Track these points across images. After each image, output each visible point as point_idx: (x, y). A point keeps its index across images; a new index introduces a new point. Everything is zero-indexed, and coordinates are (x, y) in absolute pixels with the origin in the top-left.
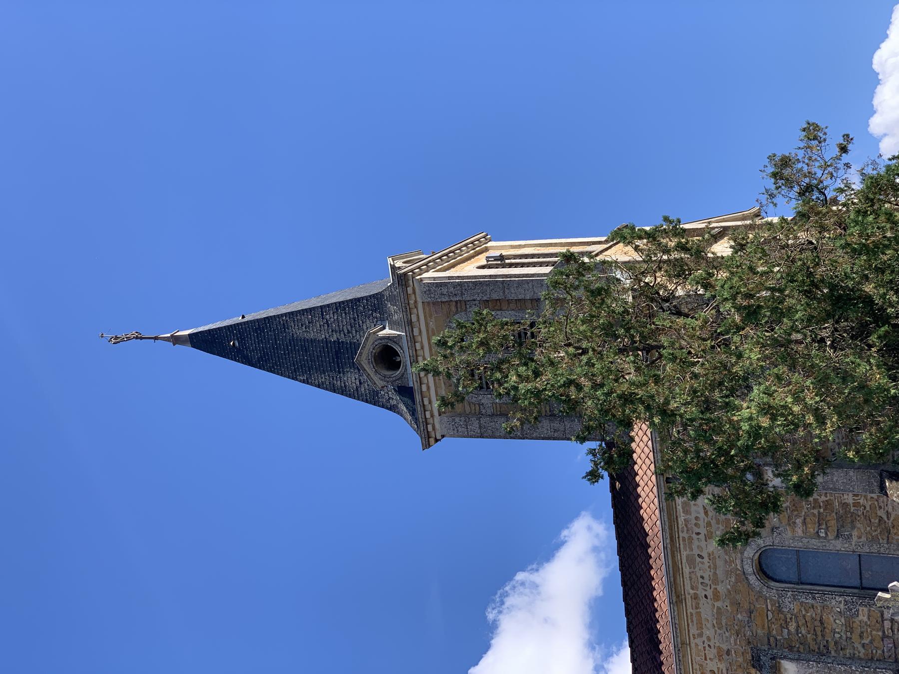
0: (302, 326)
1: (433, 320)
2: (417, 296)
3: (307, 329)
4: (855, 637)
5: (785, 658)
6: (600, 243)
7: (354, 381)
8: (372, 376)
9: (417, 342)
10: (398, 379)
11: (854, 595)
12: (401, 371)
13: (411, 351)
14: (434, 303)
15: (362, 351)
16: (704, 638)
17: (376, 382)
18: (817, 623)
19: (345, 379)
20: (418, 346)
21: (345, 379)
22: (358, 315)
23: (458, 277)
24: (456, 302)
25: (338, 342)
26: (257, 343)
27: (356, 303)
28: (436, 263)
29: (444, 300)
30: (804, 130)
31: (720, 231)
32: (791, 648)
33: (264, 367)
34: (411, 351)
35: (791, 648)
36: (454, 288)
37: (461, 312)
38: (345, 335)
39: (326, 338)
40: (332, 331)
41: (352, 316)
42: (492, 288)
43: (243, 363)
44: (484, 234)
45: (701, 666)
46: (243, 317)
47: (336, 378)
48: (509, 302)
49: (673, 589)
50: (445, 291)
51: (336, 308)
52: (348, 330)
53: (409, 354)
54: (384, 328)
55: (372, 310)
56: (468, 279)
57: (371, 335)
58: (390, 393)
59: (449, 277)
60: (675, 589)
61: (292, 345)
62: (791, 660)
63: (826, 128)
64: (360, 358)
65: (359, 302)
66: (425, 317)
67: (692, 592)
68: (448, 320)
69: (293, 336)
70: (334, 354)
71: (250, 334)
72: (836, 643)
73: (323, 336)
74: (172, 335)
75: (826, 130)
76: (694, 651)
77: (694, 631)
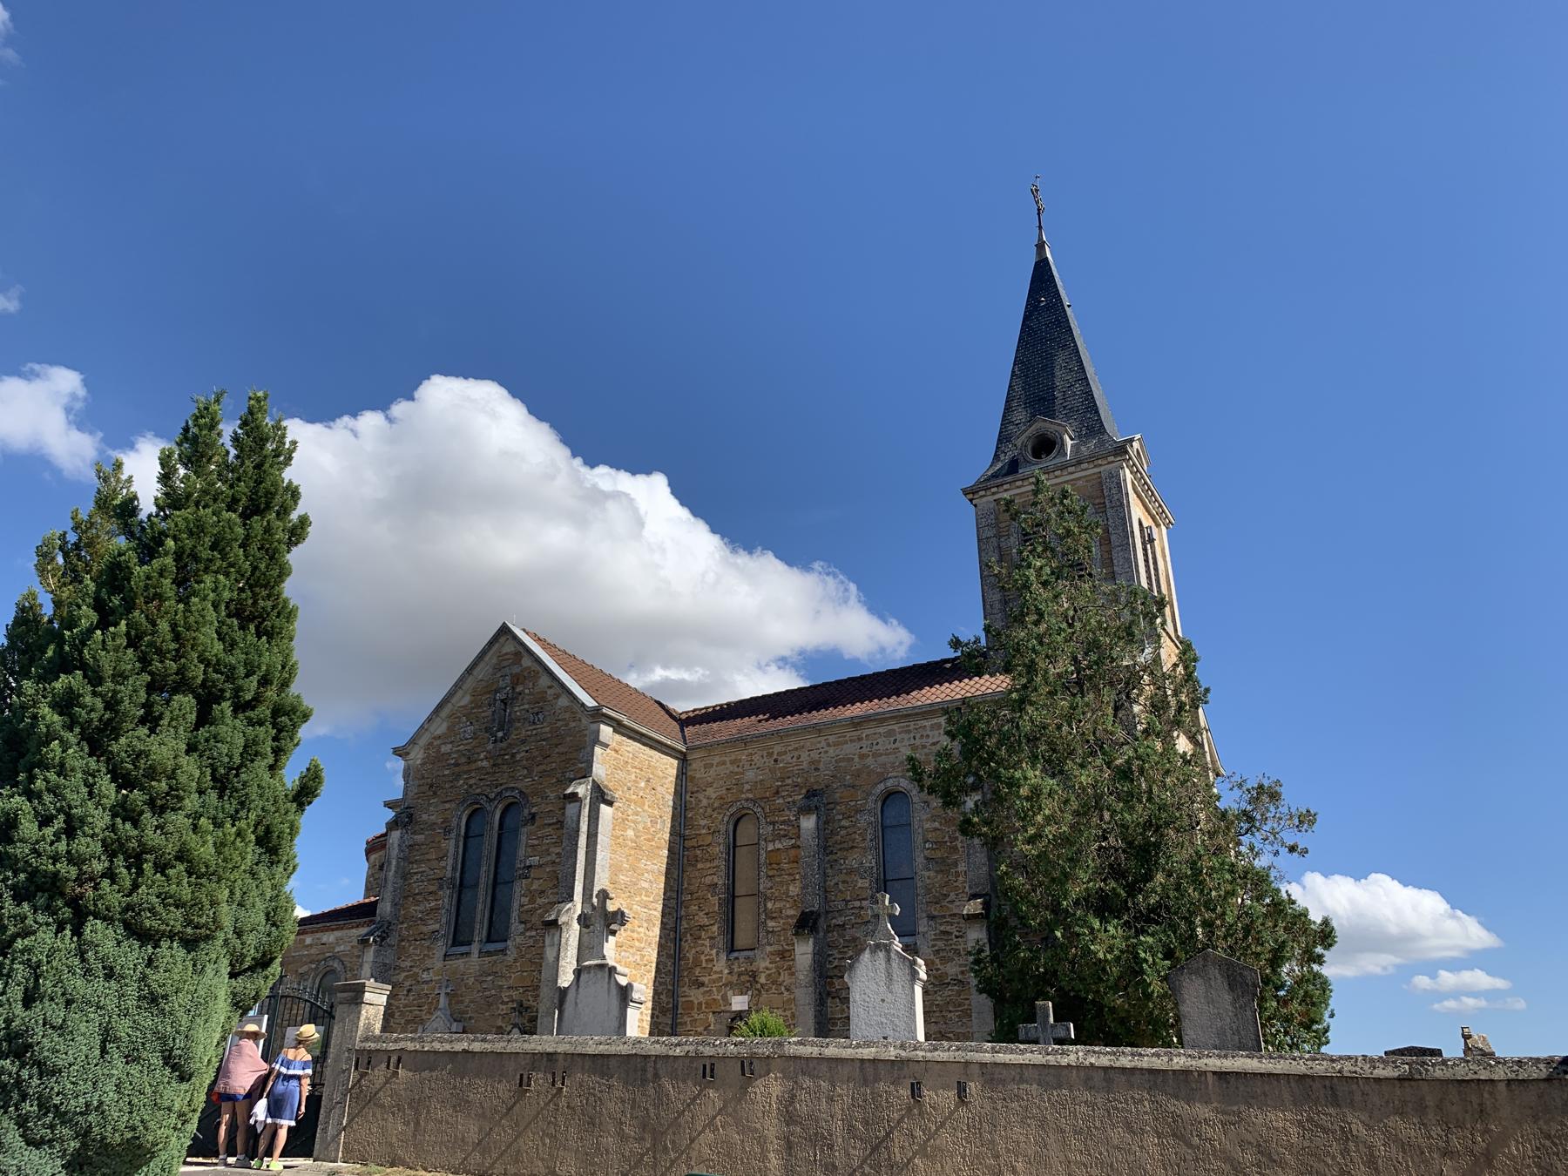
4: (843, 877)
5: (818, 818)
6: (1176, 630)
11: (878, 874)
14: (1100, 483)
18: (850, 844)
24: (1104, 503)
32: (827, 822)
35: (827, 822)
46: (1069, 306)
48: (1110, 552)
50: (1114, 491)
54: (1072, 439)
62: (817, 823)
77: (832, 739)
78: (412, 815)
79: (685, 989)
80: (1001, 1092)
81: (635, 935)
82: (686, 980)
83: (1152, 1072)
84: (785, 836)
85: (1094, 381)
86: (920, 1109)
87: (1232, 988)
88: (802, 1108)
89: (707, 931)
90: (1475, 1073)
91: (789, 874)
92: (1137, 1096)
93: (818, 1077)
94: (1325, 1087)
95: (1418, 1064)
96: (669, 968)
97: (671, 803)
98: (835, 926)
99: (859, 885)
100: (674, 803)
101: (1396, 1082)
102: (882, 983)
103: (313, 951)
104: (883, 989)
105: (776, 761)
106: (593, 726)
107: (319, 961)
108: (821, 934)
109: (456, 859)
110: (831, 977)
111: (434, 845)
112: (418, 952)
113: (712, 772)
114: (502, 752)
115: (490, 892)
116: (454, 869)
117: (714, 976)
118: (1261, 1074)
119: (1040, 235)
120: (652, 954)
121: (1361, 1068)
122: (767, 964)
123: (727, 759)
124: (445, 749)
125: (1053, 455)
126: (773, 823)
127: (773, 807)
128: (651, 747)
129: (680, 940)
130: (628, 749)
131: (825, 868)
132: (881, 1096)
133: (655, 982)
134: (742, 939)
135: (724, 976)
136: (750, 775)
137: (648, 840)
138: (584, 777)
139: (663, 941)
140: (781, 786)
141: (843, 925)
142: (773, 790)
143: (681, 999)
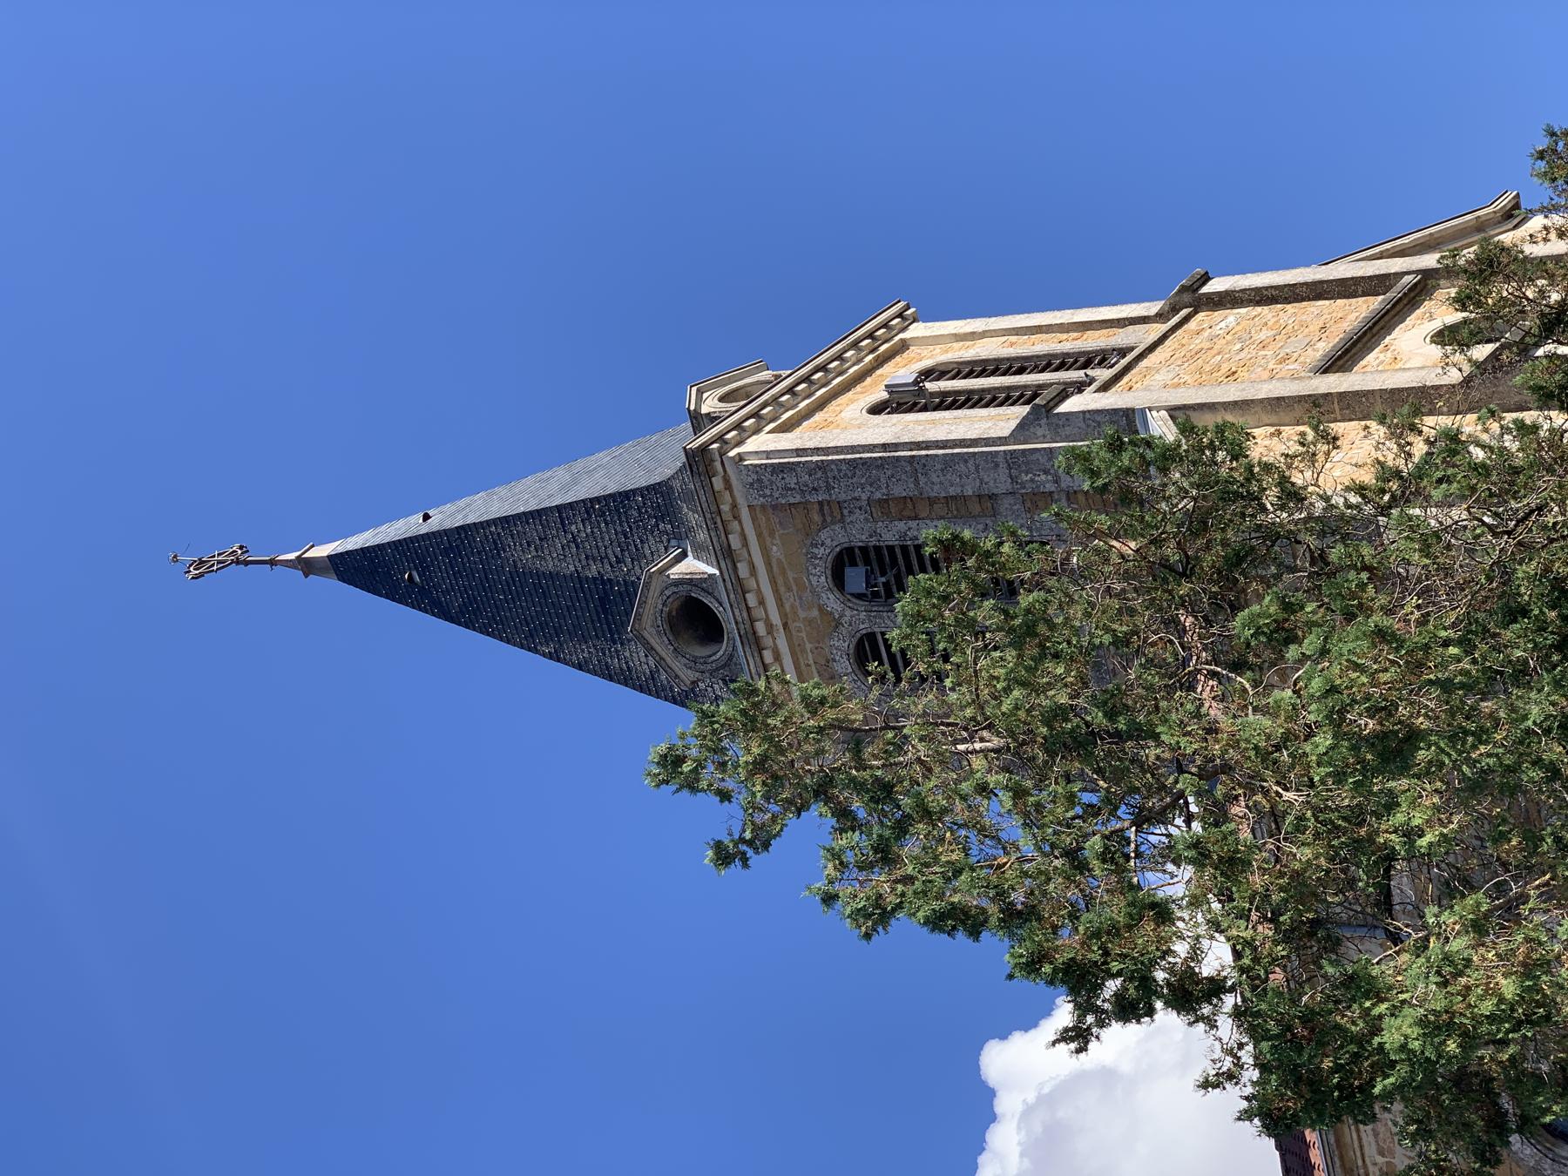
0: (529, 545)
1: (777, 541)
2: (736, 493)
3: (540, 553)
7: (643, 659)
8: (668, 660)
9: (749, 592)
10: (723, 667)
12: (726, 650)
13: (737, 612)
14: (774, 507)
15: (641, 610)
17: (680, 673)
19: (627, 654)
20: (752, 600)
21: (627, 654)
22: (630, 527)
23: (817, 451)
24: (820, 503)
25: (600, 580)
26: (452, 578)
27: (622, 502)
28: (781, 405)
29: (792, 500)
30: (1541, 155)
31: (1416, 284)
33: (474, 626)
34: (737, 612)
36: (810, 475)
37: (833, 523)
38: (612, 566)
39: (577, 571)
40: (587, 558)
41: (619, 529)
42: (889, 473)
46: (426, 517)
47: (610, 651)
48: (932, 501)
49: (1336, 1159)
50: (791, 481)
51: (587, 512)
52: (617, 557)
53: (735, 618)
54: (684, 555)
55: (656, 518)
56: (838, 453)
58: (716, 686)
59: (797, 450)
60: (1341, 1158)
61: (518, 584)
64: (639, 625)
65: (629, 500)
66: (759, 536)
67: (1380, 1159)
68: (808, 542)
69: (516, 566)
70: (597, 603)
71: (437, 559)
73: (572, 568)
85: (565, 488)
119: (287, 563)
125: (714, 606)
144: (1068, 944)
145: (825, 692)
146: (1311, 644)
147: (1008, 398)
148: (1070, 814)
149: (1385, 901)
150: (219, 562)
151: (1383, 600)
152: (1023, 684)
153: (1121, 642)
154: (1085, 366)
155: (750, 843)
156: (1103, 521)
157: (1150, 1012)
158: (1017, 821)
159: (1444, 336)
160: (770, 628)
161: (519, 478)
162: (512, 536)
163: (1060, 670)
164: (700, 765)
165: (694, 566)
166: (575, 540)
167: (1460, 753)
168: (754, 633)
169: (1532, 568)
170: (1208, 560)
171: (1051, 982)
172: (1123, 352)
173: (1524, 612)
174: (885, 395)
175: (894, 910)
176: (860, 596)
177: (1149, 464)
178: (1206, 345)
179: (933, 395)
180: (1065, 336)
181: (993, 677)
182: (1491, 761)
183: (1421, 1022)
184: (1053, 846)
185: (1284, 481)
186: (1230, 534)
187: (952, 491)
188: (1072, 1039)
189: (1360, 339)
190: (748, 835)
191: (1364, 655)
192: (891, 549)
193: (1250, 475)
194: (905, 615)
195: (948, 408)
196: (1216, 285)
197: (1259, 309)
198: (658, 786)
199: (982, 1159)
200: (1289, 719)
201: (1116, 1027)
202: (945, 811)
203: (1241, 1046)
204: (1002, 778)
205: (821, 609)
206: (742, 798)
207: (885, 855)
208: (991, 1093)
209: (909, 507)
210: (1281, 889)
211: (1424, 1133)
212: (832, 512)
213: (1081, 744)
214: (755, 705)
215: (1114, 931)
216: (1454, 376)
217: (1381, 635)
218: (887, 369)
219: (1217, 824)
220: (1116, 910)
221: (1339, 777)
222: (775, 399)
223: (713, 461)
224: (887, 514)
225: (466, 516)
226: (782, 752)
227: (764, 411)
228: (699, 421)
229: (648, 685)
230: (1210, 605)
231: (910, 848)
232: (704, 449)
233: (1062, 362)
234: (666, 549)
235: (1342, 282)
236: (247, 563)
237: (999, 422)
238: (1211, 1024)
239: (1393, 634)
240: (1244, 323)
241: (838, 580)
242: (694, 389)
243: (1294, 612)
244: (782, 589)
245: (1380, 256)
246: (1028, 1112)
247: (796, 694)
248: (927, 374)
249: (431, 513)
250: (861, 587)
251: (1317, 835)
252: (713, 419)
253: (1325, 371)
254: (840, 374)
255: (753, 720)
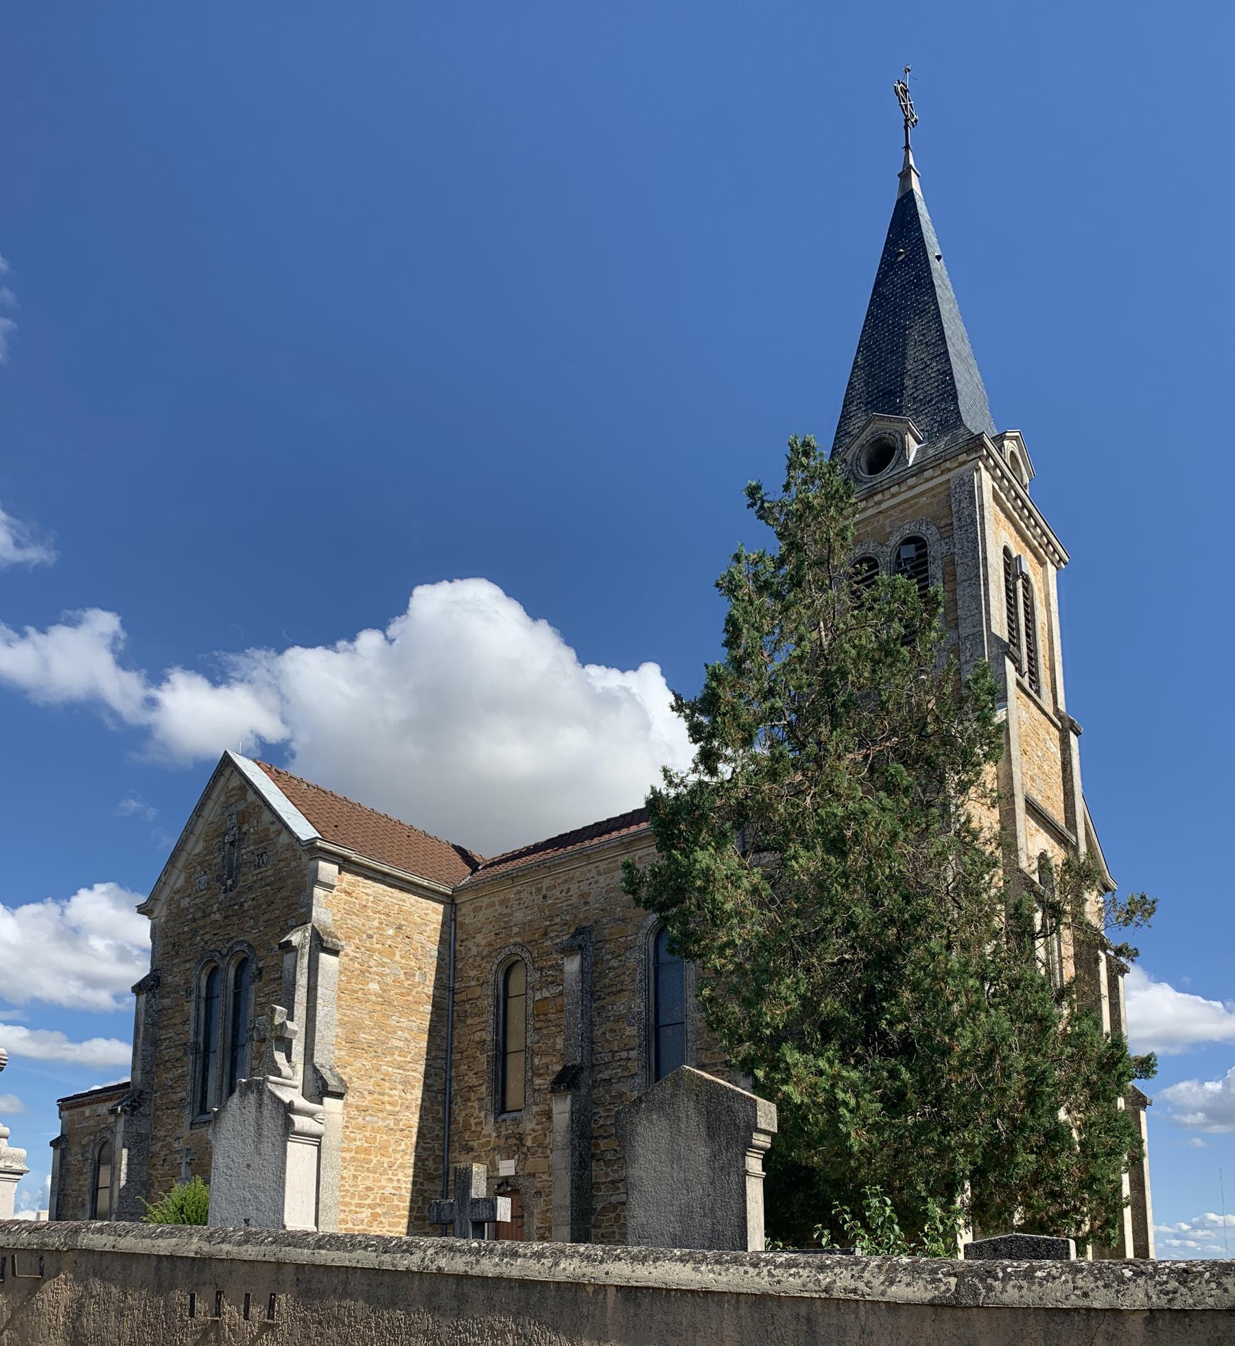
1: (929, 501)
4: (610, 1025)
5: (583, 959)
6: (1055, 702)
11: (648, 1020)
14: (949, 495)
16: (597, 878)
18: (619, 987)
20: (894, 489)
23: (983, 517)
24: (952, 524)
28: (1009, 492)
32: (595, 964)
35: (595, 964)
37: (940, 533)
43: (878, 275)
44: (1067, 559)
45: (573, 879)
46: (939, 258)
48: (954, 591)
51: (944, 372)
54: (919, 442)
57: (906, 425)
62: (582, 964)
63: (1149, 926)
66: (932, 488)
67: (636, 858)
72: (603, 1007)
73: (910, 367)
74: (911, 166)
75: (1145, 926)
76: (584, 868)
77: (602, 866)
78: (159, 977)
79: (455, 1154)
80: (317, 1311)
81: (386, 1098)
82: (457, 1144)
83: (525, 1284)
84: (552, 983)
85: (959, 354)
86: (217, 1334)
87: (712, 1134)
88: (88, 1324)
89: (476, 1092)
90: (1086, 1295)
91: (557, 1026)
92: (497, 1326)
93: (111, 1281)
94: (797, 1317)
95: (977, 1275)
96: (437, 1132)
97: (436, 953)
98: (601, 1080)
99: (627, 1033)
100: (439, 952)
101: (930, 1310)
102: (249, 1141)
103: (92, 1122)
104: (250, 1149)
105: (545, 897)
106: (312, 863)
107: (96, 1133)
108: (584, 1091)
109: (197, 1023)
110: (596, 1138)
111: (178, 1008)
112: (170, 1121)
113: (481, 916)
114: (232, 902)
115: (228, 1055)
116: (197, 1034)
117: (483, 1140)
118: (692, 1291)
120: (413, 1119)
121: (867, 1284)
122: (533, 1125)
123: (496, 900)
124: (185, 903)
125: (890, 466)
126: (541, 969)
127: (541, 951)
128: (402, 889)
129: (451, 1102)
130: (367, 891)
131: (592, 1016)
132: (174, 1311)
133: (417, 1147)
134: (511, 1103)
135: (493, 1140)
136: (519, 916)
137: (402, 994)
138: (305, 923)
139: (427, 1104)
140: (550, 926)
141: (610, 1079)
142: (541, 931)
143: (452, 1165)
144: (726, 695)
145: (850, 540)
146: (888, 802)
147: (1013, 629)
148: (791, 688)
149: (759, 850)
150: (906, 106)
151: (911, 836)
152: (859, 654)
153: (883, 705)
154: (1031, 672)
155: (762, 507)
156: (948, 689)
157: (695, 741)
158: (785, 660)
159: (1043, 856)
160: (879, 503)
161: (963, 321)
162: (928, 322)
163: (866, 674)
164: (805, 467)
165: (913, 448)
166: (926, 366)
167: (836, 878)
168: (876, 494)
169: (931, 905)
170: (928, 748)
171: (706, 686)
172: (1038, 692)
173: (908, 903)
174: (1014, 555)
175: (735, 596)
176: (898, 556)
177: (981, 710)
178: (1041, 738)
179: (1015, 584)
180: (1047, 658)
181: (860, 637)
182: (834, 892)
183: (708, 868)
184: (775, 680)
185: (971, 782)
186: (942, 758)
187: (960, 602)
188: (677, 703)
189: (1043, 817)
190: (766, 505)
191: (884, 828)
192: (926, 570)
193: (975, 765)
194: (895, 580)
195: (1007, 595)
196: (1073, 739)
197: (1060, 764)
198: (790, 444)
199: (603, 667)
200: (848, 795)
201: (686, 725)
202: (788, 618)
203: (685, 786)
204: (808, 649)
205: (891, 533)
206: (787, 499)
207: (763, 587)
208: (636, 669)
209: (950, 578)
210: (763, 799)
211: (654, 875)
212: (947, 532)
213: (828, 689)
214: (841, 497)
215: (736, 717)
216: (1023, 864)
217: (894, 836)
218: (1030, 555)
219: (792, 765)
220: (746, 718)
221: (819, 823)
222: (1012, 487)
223: (976, 452)
224: (946, 565)
225: (940, 287)
226: (815, 518)
227: (1005, 481)
228: (999, 439)
229: (842, 432)
230: (904, 751)
231: (768, 601)
232: (983, 445)
233: (1033, 659)
234: (922, 430)
235: (1074, 805)
236: (906, 127)
237: (999, 626)
238: (695, 771)
239: (895, 841)
240: (1052, 757)
241: (908, 541)
242: (1018, 434)
243: (904, 793)
244: (901, 508)
245: (1086, 824)
246: (627, 690)
247: (847, 522)
248: (1026, 580)
249: (942, 260)
250: (904, 556)
251: (790, 814)
252: (1000, 448)
253: (1026, 801)
254: (1027, 527)
255: (833, 498)
